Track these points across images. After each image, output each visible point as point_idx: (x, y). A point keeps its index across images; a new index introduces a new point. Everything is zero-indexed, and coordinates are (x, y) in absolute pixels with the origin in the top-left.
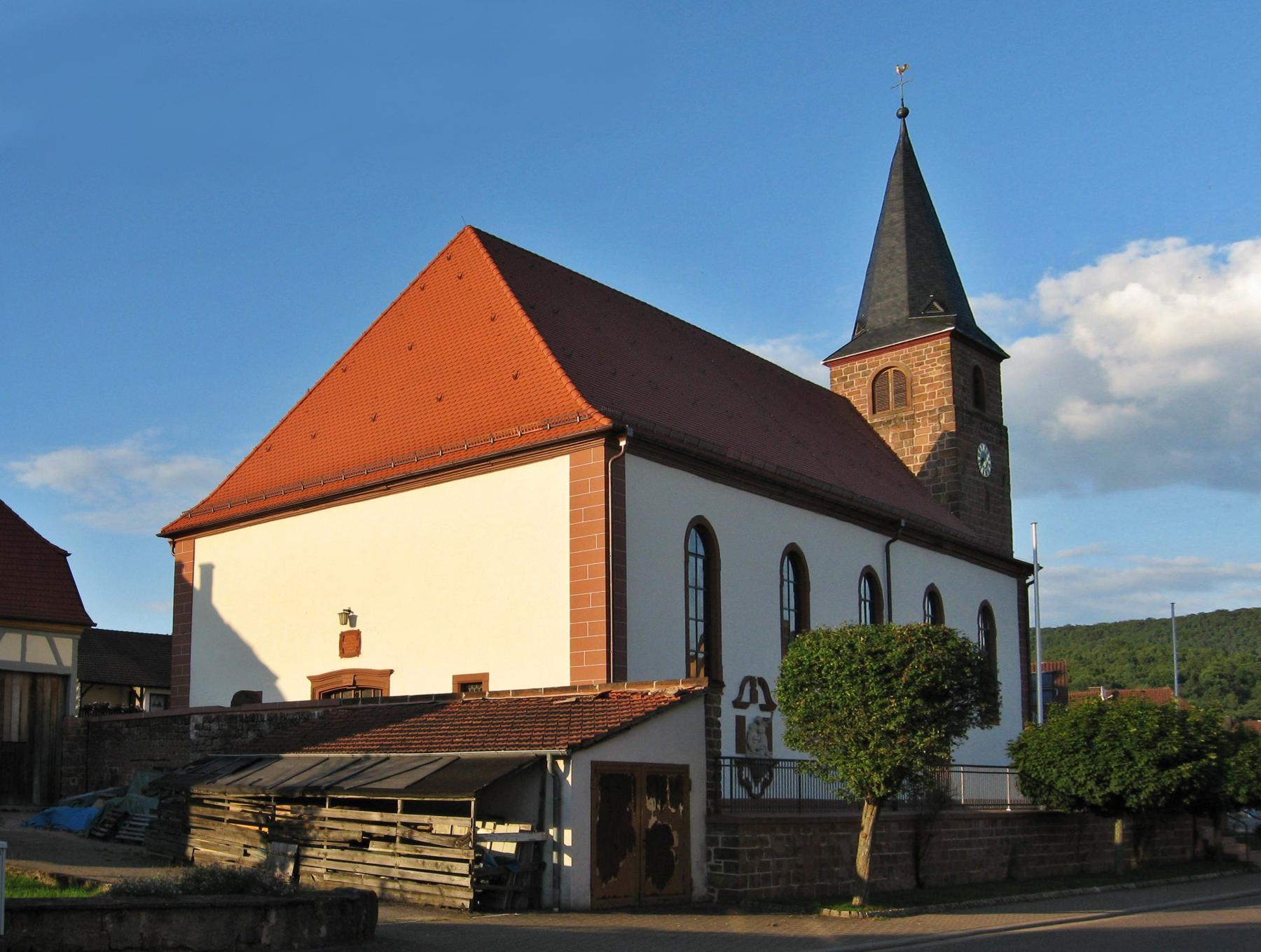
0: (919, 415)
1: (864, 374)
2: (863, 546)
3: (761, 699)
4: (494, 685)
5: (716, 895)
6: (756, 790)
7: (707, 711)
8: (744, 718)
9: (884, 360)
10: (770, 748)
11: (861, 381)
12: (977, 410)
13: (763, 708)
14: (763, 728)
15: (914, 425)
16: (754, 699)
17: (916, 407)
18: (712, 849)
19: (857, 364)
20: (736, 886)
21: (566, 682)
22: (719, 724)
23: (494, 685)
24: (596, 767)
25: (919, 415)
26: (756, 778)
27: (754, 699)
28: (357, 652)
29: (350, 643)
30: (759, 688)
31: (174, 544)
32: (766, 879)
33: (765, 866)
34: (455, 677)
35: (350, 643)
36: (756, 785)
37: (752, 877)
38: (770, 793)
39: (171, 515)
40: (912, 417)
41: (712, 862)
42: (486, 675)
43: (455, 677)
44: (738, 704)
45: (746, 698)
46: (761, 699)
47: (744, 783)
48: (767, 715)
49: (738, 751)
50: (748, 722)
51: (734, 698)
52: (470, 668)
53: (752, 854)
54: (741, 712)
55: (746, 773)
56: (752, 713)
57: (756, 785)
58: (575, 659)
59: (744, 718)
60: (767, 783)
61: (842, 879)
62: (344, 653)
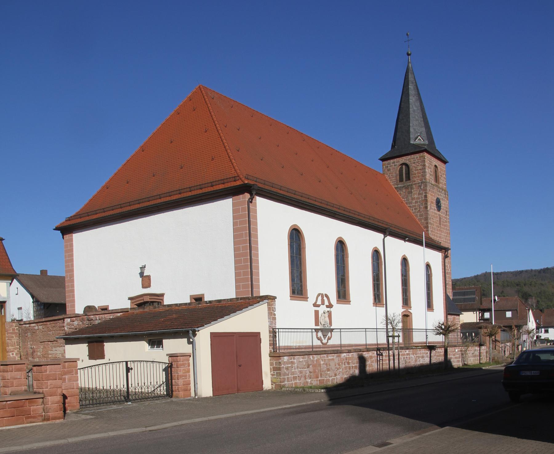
0: (414, 184)
1: (395, 166)
2: (374, 239)
3: (326, 303)
4: (167, 301)
5: (274, 386)
6: (325, 341)
7: (269, 309)
8: (318, 311)
9: (402, 160)
10: (331, 323)
11: (394, 168)
12: (437, 184)
13: (327, 307)
14: (327, 315)
15: (411, 189)
16: (323, 303)
17: (415, 181)
18: (272, 367)
19: (392, 161)
20: (281, 382)
21: (234, 296)
22: (275, 315)
23: (167, 301)
24: (214, 336)
25: (414, 184)
26: (325, 336)
27: (323, 303)
28: (149, 286)
29: (146, 281)
30: (325, 298)
31: (63, 235)
32: (295, 378)
33: (293, 373)
34: (190, 296)
35: (146, 281)
36: (325, 338)
37: (288, 378)
38: (331, 343)
39: (60, 220)
40: (412, 185)
41: (272, 373)
42: (203, 295)
43: (190, 296)
44: (315, 305)
45: (319, 302)
46: (326, 303)
47: (319, 339)
48: (329, 309)
49: (316, 325)
50: (320, 313)
51: (313, 303)
52: (197, 292)
53: (287, 369)
54: (317, 309)
55: (320, 334)
56: (322, 309)
57: (325, 338)
58: (237, 287)
59: (318, 311)
60: (329, 339)
61: (332, 376)
62: (144, 287)
